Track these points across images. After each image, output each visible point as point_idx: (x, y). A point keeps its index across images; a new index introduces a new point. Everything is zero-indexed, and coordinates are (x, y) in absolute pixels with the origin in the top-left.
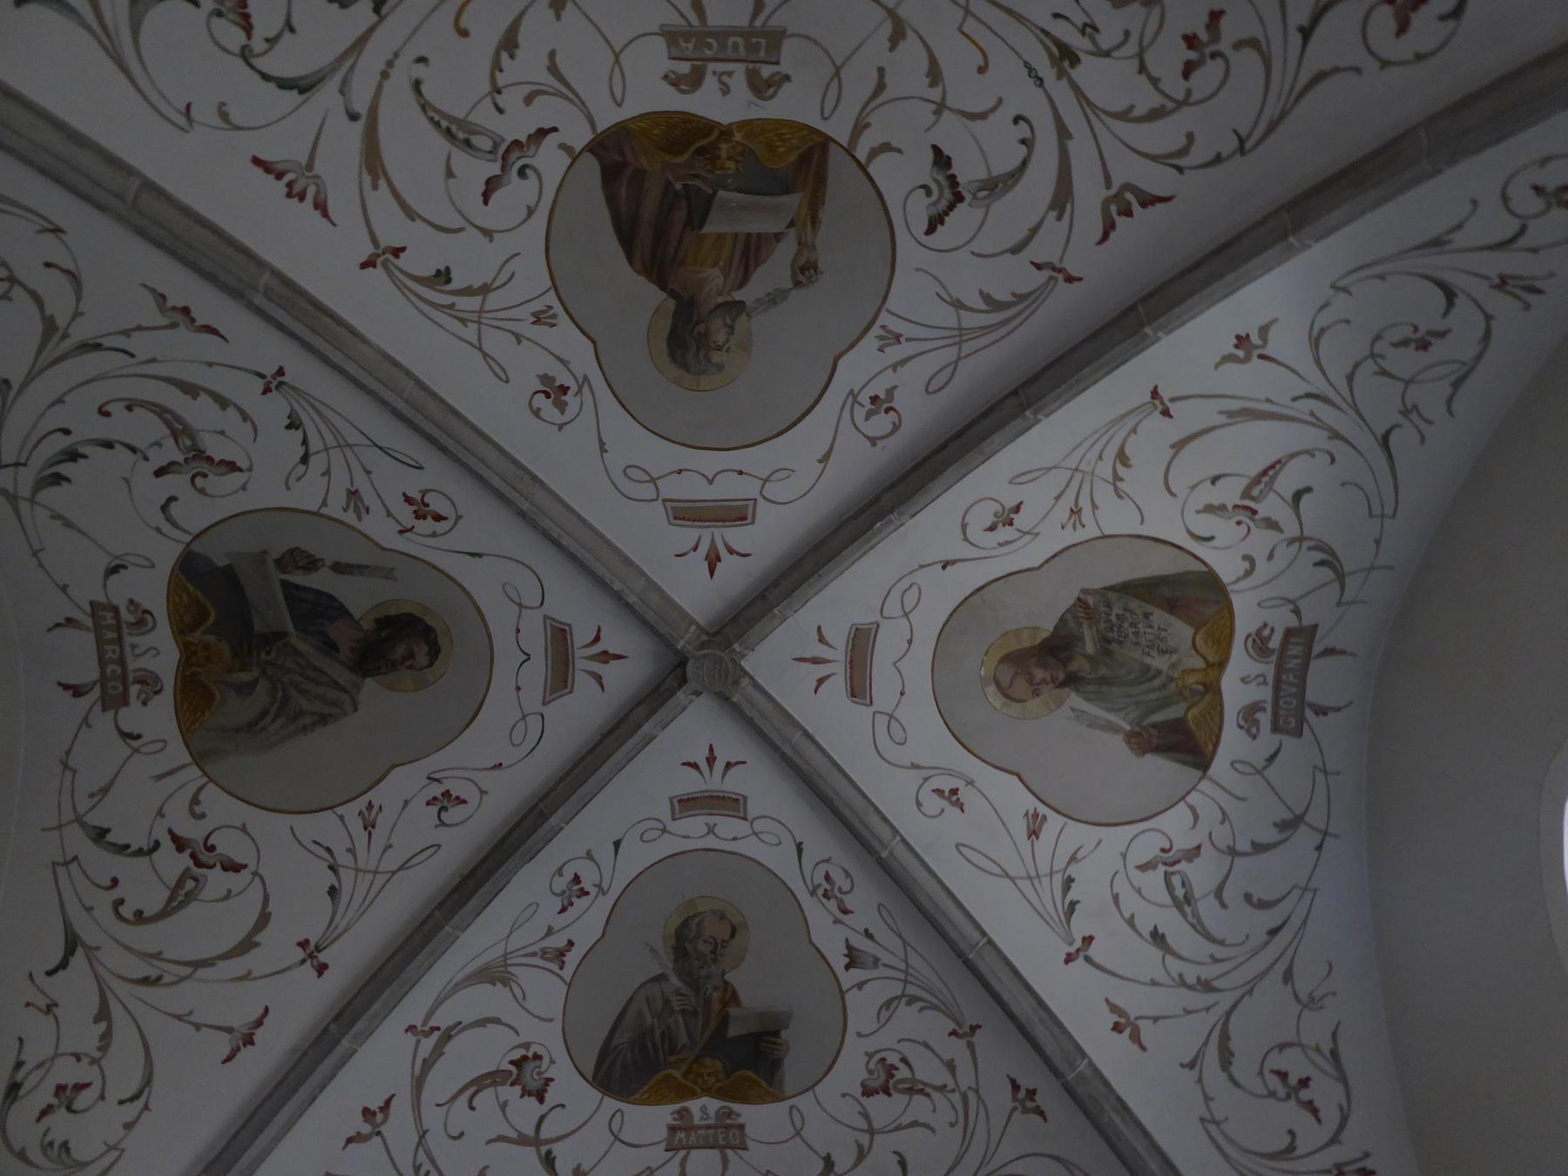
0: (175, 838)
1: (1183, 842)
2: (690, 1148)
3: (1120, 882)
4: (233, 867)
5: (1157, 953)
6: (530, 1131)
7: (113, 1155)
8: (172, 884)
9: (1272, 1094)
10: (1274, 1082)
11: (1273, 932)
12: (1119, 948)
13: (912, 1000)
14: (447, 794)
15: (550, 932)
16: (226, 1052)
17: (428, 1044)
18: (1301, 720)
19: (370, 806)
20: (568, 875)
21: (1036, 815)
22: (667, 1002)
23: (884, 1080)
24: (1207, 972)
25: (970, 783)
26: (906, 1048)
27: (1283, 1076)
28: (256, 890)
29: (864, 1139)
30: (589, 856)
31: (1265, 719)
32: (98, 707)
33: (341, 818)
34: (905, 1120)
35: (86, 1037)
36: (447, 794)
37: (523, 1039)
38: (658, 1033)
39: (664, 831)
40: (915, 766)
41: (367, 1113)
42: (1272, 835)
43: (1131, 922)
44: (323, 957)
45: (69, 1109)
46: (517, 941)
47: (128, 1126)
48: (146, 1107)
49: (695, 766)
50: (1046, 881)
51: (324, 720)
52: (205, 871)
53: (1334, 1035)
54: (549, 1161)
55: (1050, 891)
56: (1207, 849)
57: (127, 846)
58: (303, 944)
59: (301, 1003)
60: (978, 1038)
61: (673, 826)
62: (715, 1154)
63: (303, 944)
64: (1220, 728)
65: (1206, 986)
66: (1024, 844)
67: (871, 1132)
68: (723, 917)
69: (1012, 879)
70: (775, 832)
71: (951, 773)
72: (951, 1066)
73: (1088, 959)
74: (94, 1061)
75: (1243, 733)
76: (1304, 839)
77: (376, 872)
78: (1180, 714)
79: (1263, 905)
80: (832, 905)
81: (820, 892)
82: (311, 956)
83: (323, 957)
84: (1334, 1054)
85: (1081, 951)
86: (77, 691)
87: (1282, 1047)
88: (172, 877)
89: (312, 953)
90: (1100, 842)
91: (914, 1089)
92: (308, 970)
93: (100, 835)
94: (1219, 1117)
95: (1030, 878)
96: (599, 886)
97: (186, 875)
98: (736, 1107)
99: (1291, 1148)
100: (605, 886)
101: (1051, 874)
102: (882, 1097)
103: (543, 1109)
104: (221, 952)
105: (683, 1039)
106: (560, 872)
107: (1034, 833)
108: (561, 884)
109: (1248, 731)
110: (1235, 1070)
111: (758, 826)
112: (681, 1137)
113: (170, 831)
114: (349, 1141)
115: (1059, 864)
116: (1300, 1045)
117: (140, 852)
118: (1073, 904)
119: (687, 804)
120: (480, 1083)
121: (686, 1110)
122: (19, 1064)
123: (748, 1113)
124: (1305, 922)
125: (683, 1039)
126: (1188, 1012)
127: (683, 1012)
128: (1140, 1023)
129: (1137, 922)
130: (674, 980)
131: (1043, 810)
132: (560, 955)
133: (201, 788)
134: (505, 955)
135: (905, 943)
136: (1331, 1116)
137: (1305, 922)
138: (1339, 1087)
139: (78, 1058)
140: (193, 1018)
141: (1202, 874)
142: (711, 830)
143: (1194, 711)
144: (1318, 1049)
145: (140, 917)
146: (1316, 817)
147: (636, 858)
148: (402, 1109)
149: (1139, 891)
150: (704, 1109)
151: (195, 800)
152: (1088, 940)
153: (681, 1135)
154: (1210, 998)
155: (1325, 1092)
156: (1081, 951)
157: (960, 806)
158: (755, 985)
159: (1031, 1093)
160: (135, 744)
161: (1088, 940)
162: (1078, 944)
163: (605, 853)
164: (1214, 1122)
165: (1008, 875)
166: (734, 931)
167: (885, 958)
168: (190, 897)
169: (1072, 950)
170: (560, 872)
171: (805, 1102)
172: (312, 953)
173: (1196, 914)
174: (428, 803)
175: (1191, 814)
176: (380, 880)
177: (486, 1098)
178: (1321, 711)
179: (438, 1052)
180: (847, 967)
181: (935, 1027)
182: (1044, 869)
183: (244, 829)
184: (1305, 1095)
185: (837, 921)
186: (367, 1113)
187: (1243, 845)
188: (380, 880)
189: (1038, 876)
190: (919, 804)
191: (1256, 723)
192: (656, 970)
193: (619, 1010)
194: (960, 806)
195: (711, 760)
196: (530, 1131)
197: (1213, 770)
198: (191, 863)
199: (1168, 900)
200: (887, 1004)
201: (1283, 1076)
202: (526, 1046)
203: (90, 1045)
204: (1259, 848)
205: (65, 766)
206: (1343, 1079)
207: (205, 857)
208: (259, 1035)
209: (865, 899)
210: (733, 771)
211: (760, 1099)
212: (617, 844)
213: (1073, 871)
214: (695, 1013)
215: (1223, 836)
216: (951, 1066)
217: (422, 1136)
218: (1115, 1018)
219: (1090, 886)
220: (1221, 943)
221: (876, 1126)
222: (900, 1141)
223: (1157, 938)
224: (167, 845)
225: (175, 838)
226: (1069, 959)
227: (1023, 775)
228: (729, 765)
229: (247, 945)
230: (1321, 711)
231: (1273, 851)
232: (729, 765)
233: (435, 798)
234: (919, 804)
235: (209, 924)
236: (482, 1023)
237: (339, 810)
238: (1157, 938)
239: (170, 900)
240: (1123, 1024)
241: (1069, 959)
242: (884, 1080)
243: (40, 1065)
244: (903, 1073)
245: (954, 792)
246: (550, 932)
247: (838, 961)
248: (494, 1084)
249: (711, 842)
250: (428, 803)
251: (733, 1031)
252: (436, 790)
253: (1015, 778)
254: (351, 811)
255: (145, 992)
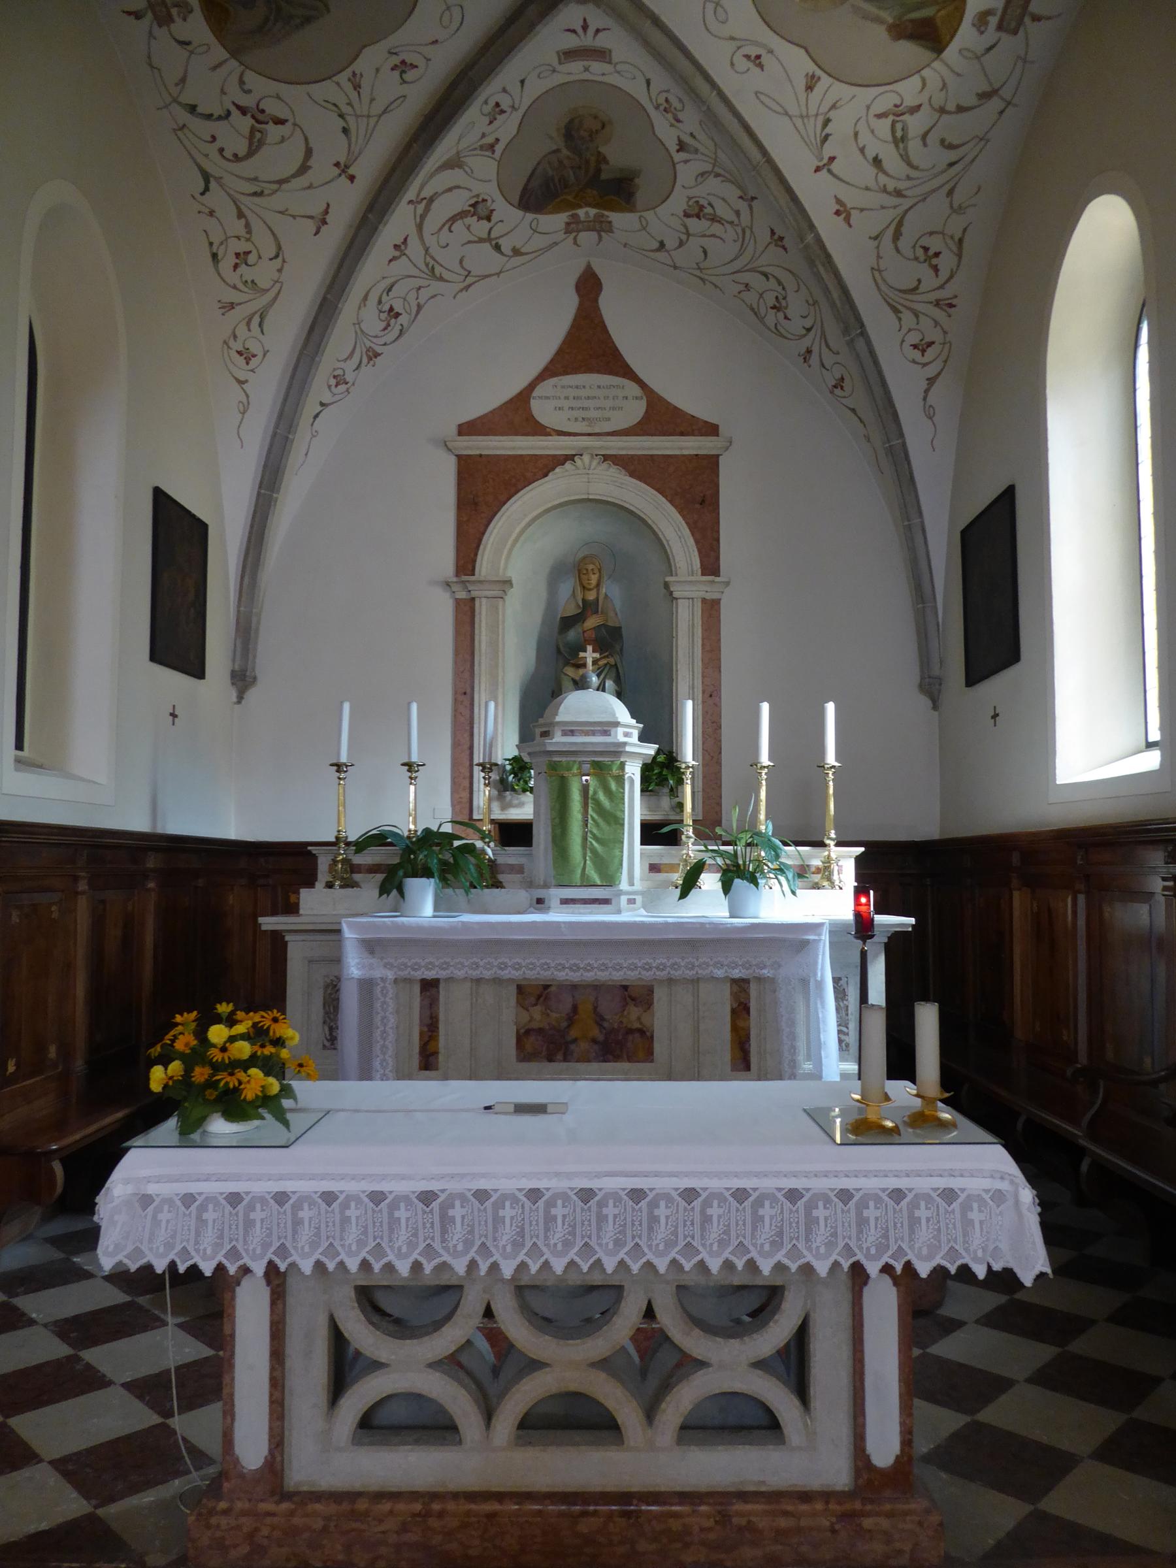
0: (238, 107)
1: (910, 102)
2: (579, 231)
3: (863, 122)
4: (280, 122)
5: (874, 171)
6: (485, 236)
7: (278, 285)
8: (247, 135)
9: (916, 259)
10: (920, 253)
11: (951, 165)
12: (852, 166)
13: (717, 175)
14: (403, 62)
15: (484, 135)
16: (314, 230)
17: (421, 208)
18: (1020, 22)
19: (354, 74)
20: (492, 103)
21: (813, 76)
22: (561, 162)
23: (697, 211)
24: (901, 185)
25: (771, 52)
26: (711, 198)
27: (926, 249)
28: (298, 137)
29: (684, 237)
30: (504, 90)
31: (993, 21)
32: (155, 26)
33: (338, 84)
34: (708, 233)
35: (238, 227)
36: (403, 62)
37: (475, 192)
38: (556, 180)
39: (554, 71)
40: (732, 38)
41: (396, 247)
42: (972, 101)
43: (862, 150)
44: (351, 171)
45: (247, 264)
46: (463, 144)
47: (280, 271)
48: (284, 261)
49: (574, 31)
50: (812, 119)
51: (308, 20)
52: (263, 126)
53: (965, 230)
54: (497, 248)
55: (813, 128)
56: (925, 108)
57: (211, 115)
58: (337, 165)
59: (347, 200)
60: (755, 203)
61: (559, 68)
62: (594, 235)
63: (337, 165)
64: (959, 25)
65: (898, 193)
66: (802, 95)
67: (688, 234)
68: (596, 117)
69: (790, 117)
70: (629, 70)
71: (756, 43)
72: (738, 213)
73: (829, 171)
74: (248, 240)
75: (974, 29)
76: (995, 104)
77: (369, 116)
78: (931, 14)
79: (951, 147)
80: (670, 116)
81: (662, 108)
82: (343, 171)
83: (351, 171)
84: (961, 241)
85: (826, 166)
86: (138, 15)
87: (931, 233)
88: (246, 131)
89: (343, 168)
90: (854, 97)
91: (714, 219)
92: (344, 179)
93: (192, 109)
94: (882, 268)
95: (802, 117)
96: (513, 107)
97: (253, 130)
98: (606, 213)
99: (916, 288)
100: (516, 106)
101: (817, 115)
102: (695, 220)
103: (491, 224)
104: (292, 172)
105: (572, 179)
106: (486, 102)
107: (810, 88)
108: (488, 109)
109: (978, 30)
110: (900, 244)
111: (619, 67)
112: (572, 227)
113: (234, 103)
114: (390, 261)
115: (823, 109)
116: (942, 233)
117: (220, 118)
118: (827, 136)
119: (569, 55)
120: (453, 219)
121: (576, 215)
122: (211, 244)
123: (615, 217)
124: (973, 161)
125: (572, 179)
126: (883, 208)
127: (572, 168)
128: (853, 212)
129: (866, 151)
130: (565, 152)
131: (819, 72)
132: (491, 147)
133: (242, 75)
134: (458, 153)
135: (716, 145)
136: (944, 274)
137: (973, 161)
138: (956, 259)
139: (238, 238)
140: (290, 212)
141: (915, 124)
142: (586, 69)
143: (943, 12)
144: (952, 237)
145: (237, 158)
146: (1006, 92)
147: (536, 87)
148: (414, 241)
149: (872, 132)
150: (587, 213)
151: (242, 82)
152: (832, 159)
153: (573, 226)
154: (895, 201)
155: (946, 262)
156: (826, 166)
157: (761, 66)
158: (617, 154)
159: (781, 239)
160: (189, 48)
161: (832, 159)
162: (825, 161)
163: (515, 89)
164: (880, 271)
165: (786, 114)
166: (603, 127)
167: (702, 149)
168: (261, 143)
169: (821, 164)
170: (486, 102)
171: (650, 215)
172: (343, 168)
173: (906, 149)
174: (392, 69)
175: (924, 82)
176: (372, 121)
177: (458, 226)
178: (1036, 18)
179: (427, 209)
180: (678, 151)
181: (732, 192)
182: (812, 111)
183: (278, 97)
184: (934, 261)
185: (672, 125)
186: (396, 247)
187: (951, 107)
188: (372, 121)
189: (807, 116)
190: (732, 64)
191: (986, 23)
192: (554, 147)
193: (529, 172)
194: (761, 66)
195: (585, 27)
196: (485, 236)
197: (946, 54)
198: (253, 121)
199: (890, 138)
200: (702, 174)
201: (926, 249)
202: (478, 196)
203: (242, 232)
204: (961, 109)
205: (152, 67)
206: (960, 256)
207: (260, 117)
208: (329, 218)
209: (691, 118)
210: (600, 34)
211: (622, 210)
212: (522, 82)
213: (832, 114)
214: (580, 168)
215: (938, 101)
216: (738, 213)
217: (427, 250)
218: (838, 207)
219: (841, 124)
220: (916, 168)
221: (691, 231)
222: (705, 242)
223: (877, 162)
224: (235, 113)
225: (238, 107)
226: (818, 170)
227: (810, 50)
228: (598, 31)
229: (304, 169)
230: (1036, 18)
231: (970, 113)
232: (598, 31)
233: (396, 66)
234: (732, 64)
235: (279, 157)
236: (450, 190)
237: (334, 79)
238: (877, 162)
239: (251, 144)
240: (843, 212)
241: (818, 170)
242: (697, 211)
243: (222, 243)
244: (709, 210)
245: (758, 57)
246: (484, 135)
247: (673, 147)
248: (462, 218)
249: (586, 76)
250: (392, 69)
251: (604, 176)
252: (396, 60)
253: (803, 51)
254: (343, 78)
255: (256, 200)
